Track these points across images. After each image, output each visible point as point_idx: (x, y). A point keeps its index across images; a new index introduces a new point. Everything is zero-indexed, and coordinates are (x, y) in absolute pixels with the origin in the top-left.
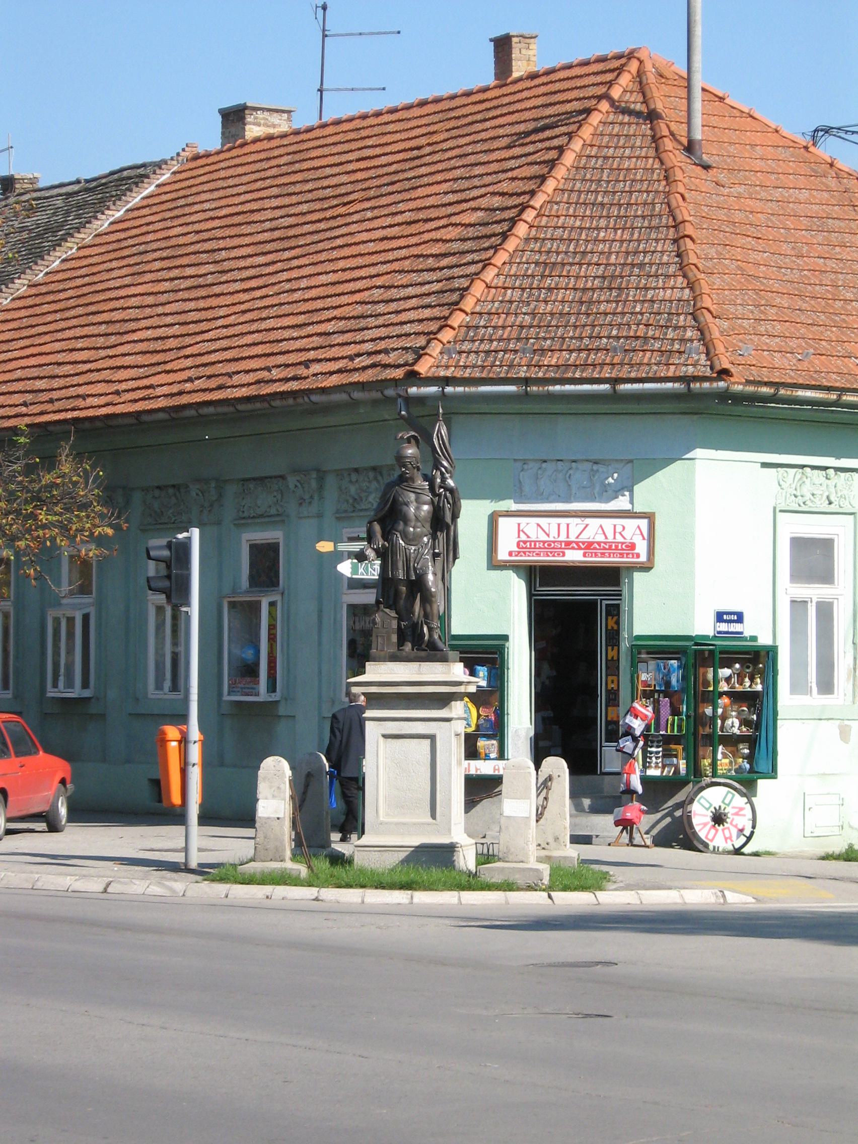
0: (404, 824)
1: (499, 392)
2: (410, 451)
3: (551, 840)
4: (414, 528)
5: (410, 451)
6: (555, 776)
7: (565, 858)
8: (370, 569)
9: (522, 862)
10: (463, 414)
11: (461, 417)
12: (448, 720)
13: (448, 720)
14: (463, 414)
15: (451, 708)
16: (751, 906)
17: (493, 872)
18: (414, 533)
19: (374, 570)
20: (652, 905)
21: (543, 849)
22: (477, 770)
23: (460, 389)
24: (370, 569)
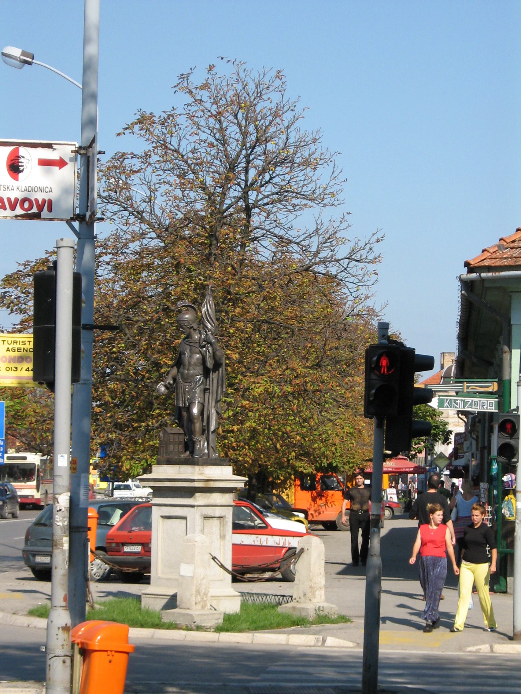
0: (170, 579)
1: (516, 275)
2: (187, 316)
3: (302, 595)
4: (188, 370)
5: (187, 316)
6: (305, 549)
7: (303, 609)
8: (453, 403)
9: (188, 609)
10: (518, 292)
11: (517, 294)
12: (193, 506)
13: (193, 506)
14: (518, 292)
15: (195, 498)
16: (488, 654)
17: (168, 616)
18: (188, 374)
19: (457, 404)
20: (266, 645)
21: (297, 602)
22: (289, 543)
23: (490, 274)
24: (453, 403)
